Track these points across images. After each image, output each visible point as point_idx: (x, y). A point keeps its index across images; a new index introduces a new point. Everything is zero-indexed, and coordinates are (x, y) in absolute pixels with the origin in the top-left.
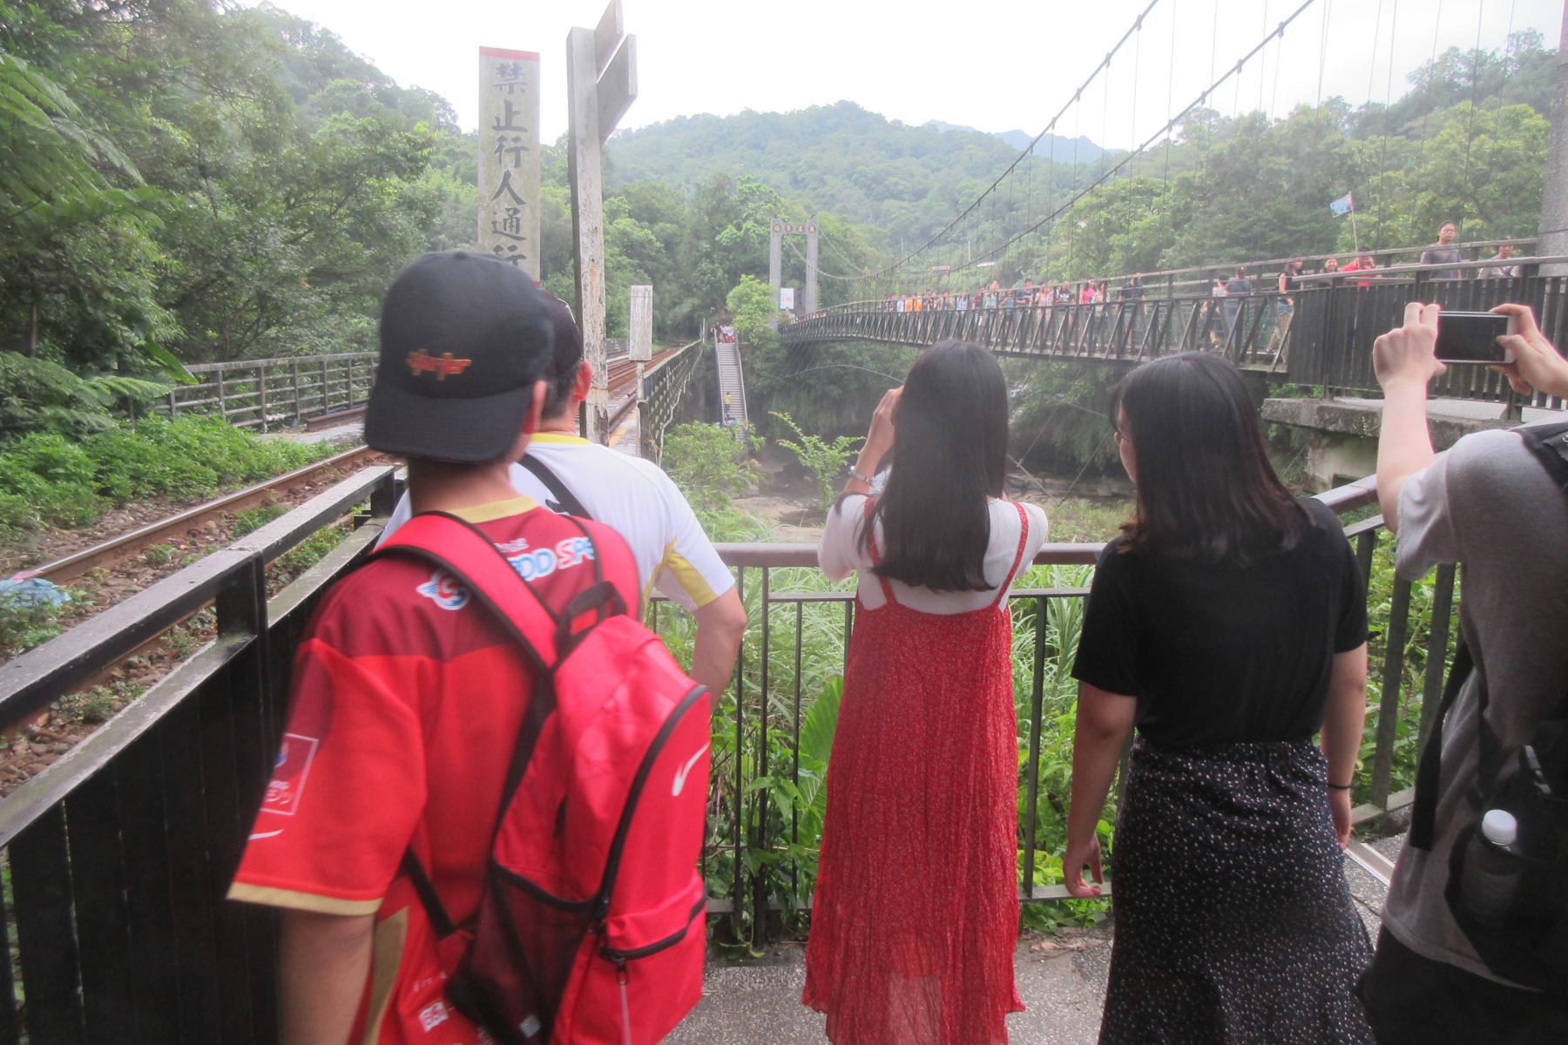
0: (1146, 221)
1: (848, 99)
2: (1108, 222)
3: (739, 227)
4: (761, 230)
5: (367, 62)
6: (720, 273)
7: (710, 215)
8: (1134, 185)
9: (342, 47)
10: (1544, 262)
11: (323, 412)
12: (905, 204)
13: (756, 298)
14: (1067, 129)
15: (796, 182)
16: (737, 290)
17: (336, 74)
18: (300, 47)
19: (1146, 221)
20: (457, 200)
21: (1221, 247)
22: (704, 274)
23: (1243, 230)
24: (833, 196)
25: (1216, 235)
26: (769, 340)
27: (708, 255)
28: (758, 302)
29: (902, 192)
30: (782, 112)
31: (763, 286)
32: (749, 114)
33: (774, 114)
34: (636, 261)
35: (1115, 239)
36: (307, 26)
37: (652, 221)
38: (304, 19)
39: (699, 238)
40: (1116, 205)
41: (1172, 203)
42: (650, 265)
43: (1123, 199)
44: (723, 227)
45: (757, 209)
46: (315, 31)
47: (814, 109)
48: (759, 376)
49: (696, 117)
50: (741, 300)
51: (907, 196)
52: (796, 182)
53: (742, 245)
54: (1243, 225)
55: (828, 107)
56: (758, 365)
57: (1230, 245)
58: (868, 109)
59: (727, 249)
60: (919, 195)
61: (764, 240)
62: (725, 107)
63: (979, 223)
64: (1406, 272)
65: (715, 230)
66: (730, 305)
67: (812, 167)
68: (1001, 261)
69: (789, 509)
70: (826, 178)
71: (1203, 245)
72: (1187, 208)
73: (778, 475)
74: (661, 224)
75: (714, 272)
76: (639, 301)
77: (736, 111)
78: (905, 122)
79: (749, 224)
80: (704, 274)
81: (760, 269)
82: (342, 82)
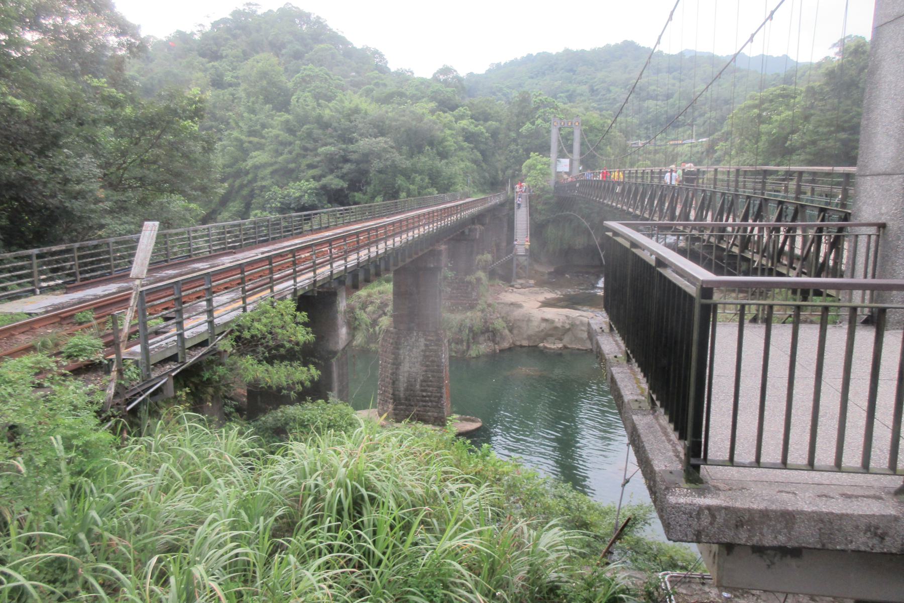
0: (783, 115)
1: (629, 39)
2: (759, 116)
3: (533, 123)
4: (547, 125)
5: (340, 34)
6: (520, 152)
7: (518, 116)
8: (778, 92)
9: (326, 25)
10: (851, 226)
11: (74, 281)
12: (659, 103)
13: (539, 167)
14: (753, 51)
15: (593, 91)
16: (528, 162)
17: (321, 42)
18: (304, 27)
19: (783, 115)
20: (366, 113)
21: (831, 133)
22: (511, 152)
23: (845, 122)
24: (614, 99)
25: (828, 125)
26: (547, 192)
27: (515, 140)
28: (540, 169)
29: (657, 95)
30: (588, 49)
31: (545, 159)
32: (567, 52)
33: (583, 51)
34: (472, 145)
35: (764, 128)
36: (308, 16)
37: (486, 120)
38: (307, 11)
39: (510, 130)
40: (766, 105)
41: (803, 103)
42: (482, 147)
43: (771, 101)
44: (524, 123)
45: (544, 113)
46: (312, 17)
47: (608, 46)
48: (540, 213)
49: (539, 54)
50: (530, 168)
51: (660, 97)
52: (593, 91)
53: (535, 134)
54: (846, 118)
55: (617, 45)
56: (539, 207)
57: (837, 131)
58: (601, 46)
59: (526, 137)
60: (668, 97)
61: (549, 131)
62: (555, 48)
63: (705, 113)
64: (652, 252)
65: (519, 125)
66: (524, 171)
67: (604, 82)
68: (711, 137)
69: (550, 295)
70: (611, 88)
71: (817, 132)
72: (812, 107)
73: (550, 273)
74: (490, 122)
75: (517, 151)
76: (147, 233)
77: (561, 50)
78: (665, 52)
79: (539, 121)
80: (511, 152)
81: (544, 149)
82: (322, 46)
